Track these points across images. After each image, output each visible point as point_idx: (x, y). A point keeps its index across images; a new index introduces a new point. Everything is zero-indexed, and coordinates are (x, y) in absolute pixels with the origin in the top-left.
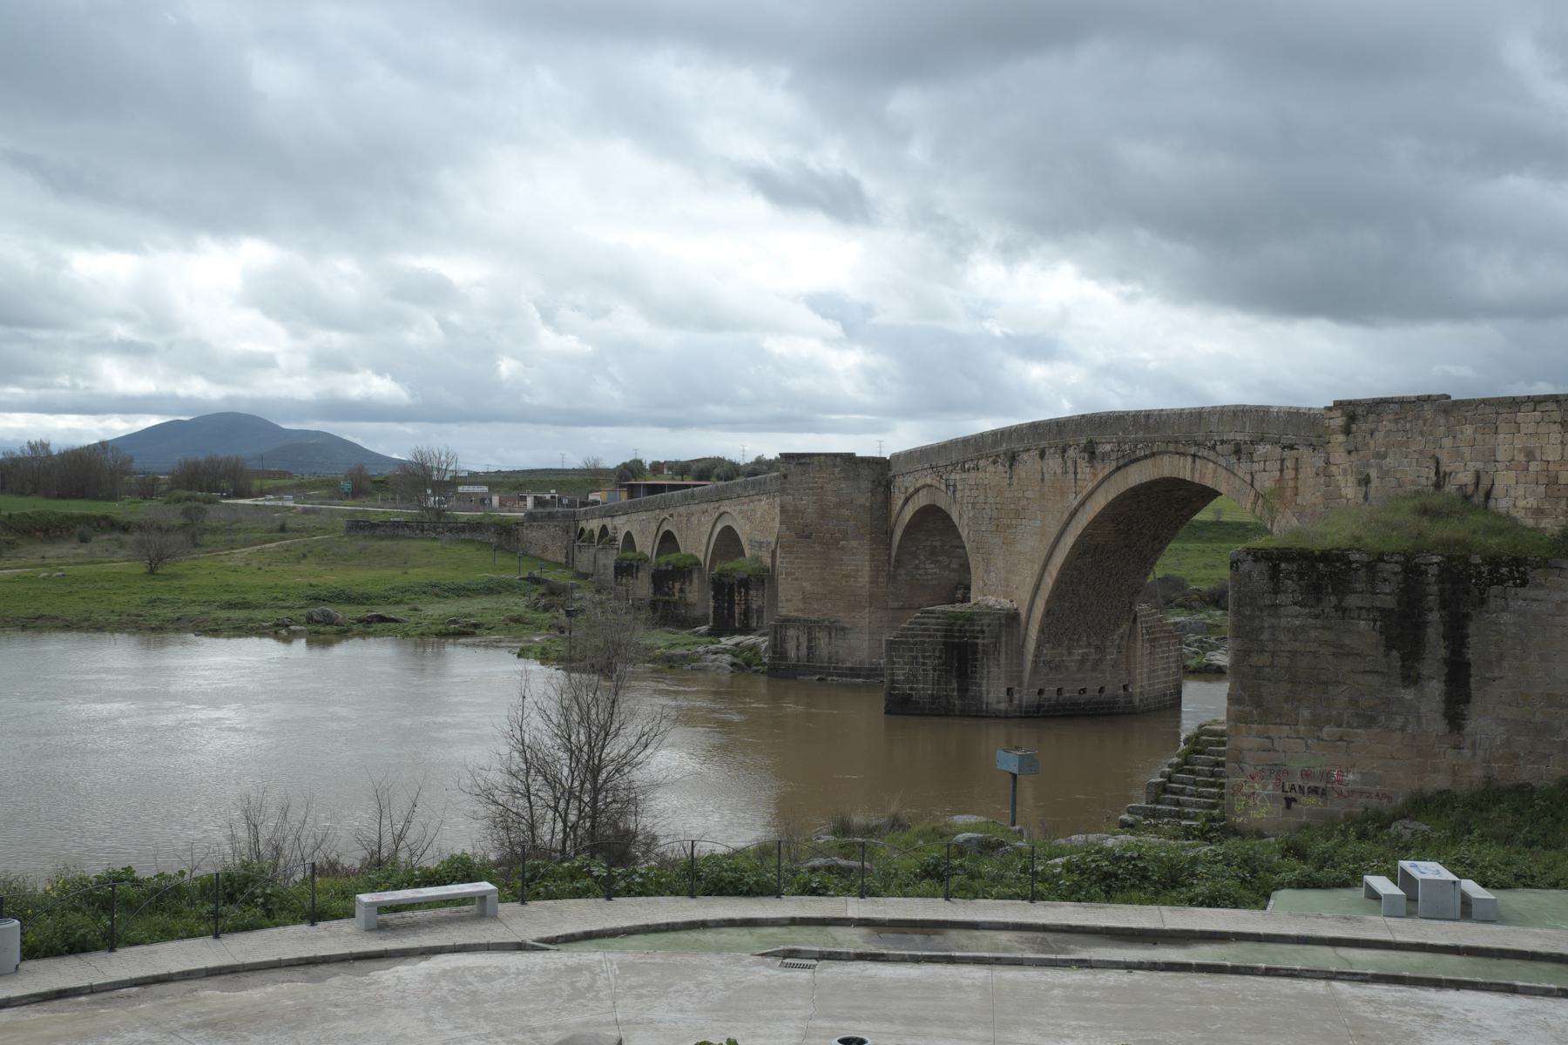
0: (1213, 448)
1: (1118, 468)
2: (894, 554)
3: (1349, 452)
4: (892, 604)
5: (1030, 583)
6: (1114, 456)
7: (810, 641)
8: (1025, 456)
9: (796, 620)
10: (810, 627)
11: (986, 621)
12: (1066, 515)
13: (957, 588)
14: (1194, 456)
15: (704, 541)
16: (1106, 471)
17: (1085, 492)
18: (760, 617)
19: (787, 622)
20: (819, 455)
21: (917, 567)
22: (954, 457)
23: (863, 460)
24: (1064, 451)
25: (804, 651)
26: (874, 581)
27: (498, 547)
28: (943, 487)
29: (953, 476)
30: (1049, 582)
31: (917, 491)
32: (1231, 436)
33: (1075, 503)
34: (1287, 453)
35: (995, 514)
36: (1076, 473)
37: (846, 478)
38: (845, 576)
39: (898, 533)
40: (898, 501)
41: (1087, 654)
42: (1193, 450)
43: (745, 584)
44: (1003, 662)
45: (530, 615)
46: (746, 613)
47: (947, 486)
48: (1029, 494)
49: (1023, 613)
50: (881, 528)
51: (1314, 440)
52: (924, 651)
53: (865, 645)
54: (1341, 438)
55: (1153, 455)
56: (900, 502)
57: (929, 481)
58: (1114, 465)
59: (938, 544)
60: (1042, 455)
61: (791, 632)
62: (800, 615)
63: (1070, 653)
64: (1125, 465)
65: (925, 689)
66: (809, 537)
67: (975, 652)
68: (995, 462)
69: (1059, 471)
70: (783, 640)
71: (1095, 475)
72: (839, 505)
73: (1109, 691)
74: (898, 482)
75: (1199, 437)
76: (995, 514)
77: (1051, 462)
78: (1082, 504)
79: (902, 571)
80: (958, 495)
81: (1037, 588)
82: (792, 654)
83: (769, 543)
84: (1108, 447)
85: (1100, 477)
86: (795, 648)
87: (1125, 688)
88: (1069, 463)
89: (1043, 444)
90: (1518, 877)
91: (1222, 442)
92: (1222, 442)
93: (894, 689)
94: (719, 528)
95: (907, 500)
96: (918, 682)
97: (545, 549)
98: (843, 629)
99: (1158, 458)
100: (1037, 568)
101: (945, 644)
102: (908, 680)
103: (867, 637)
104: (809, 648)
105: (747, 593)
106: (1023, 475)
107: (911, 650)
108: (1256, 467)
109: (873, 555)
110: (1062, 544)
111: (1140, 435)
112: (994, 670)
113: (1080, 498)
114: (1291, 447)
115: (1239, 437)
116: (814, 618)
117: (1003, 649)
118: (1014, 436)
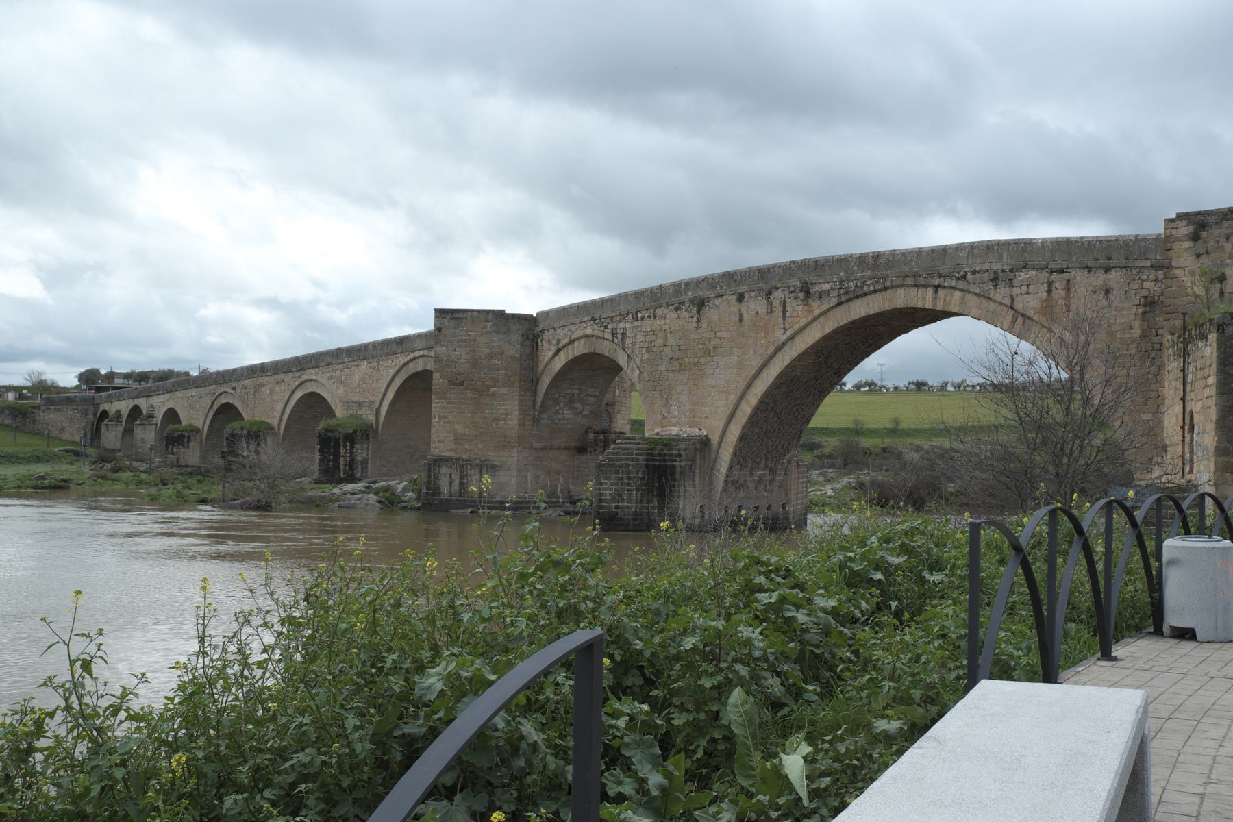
0: (964, 277)
1: (839, 304)
2: (539, 400)
3: (1198, 256)
4: (536, 445)
5: (723, 411)
6: (836, 293)
7: (462, 477)
8: (718, 302)
9: (449, 459)
10: (462, 465)
11: (683, 446)
12: (771, 349)
13: (587, 432)
14: (937, 287)
15: (279, 408)
16: (824, 308)
17: (796, 327)
18: (364, 468)
19: (440, 461)
20: (472, 311)
21: (557, 413)
22: (623, 309)
23: (514, 316)
24: (769, 293)
25: (456, 487)
26: (522, 424)
27: (17, 429)
28: (609, 336)
29: (621, 325)
30: (747, 409)
31: (572, 342)
32: (986, 266)
33: (784, 337)
34: (1055, 276)
35: (678, 354)
36: (784, 311)
37: (498, 332)
38: (495, 419)
39: (545, 381)
40: (547, 352)
41: (763, 475)
42: (937, 281)
43: (351, 438)
44: (697, 482)
45: (110, 474)
46: (351, 465)
47: (613, 335)
48: (723, 334)
49: (715, 440)
50: (529, 380)
51: (1090, 263)
52: (629, 472)
53: (514, 481)
54: (1187, 244)
55: (885, 289)
56: (551, 354)
57: (589, 331)
58: (835, 301)
59: (576, 392)
60: (741, 298)
61: (444, 470)
62: (453, 454)
63: (751, 474)
64: (848, 301)
65: (629, 507)
66: (462, 384)
67: (673, 474)
68: (677, 309)
69: (762, 311)
70: (437, 478)
71: (810, 312)
72: (490, 356)
73: (774, 509)
74: (548, 335)
75: (945, 270)
76: (678, 354)
77: (752, 305)
78: (792, 338)
79: (545, 416)
80: (627, 341)
81: (732, 416)
82: (445, 490)
83: (372, 402)
84: (827, 287)
85: (816, 312)
86: (447, 484)
87: (784, 508)
88: (776, 303)
89: (741, 289)
90: (928, 700)
91: (974, 272)
92: (974, 272)
93: (601, 507)
94: (298, 394)
95: (558, 351)
96: (623, 501)
97: (62, 430)
98: (494, 467)
99: (889, 292)
100: (733, 398)
101: (647, 466)
102: (614, 500)
103: (515, 474)
104: (462, 484)
105: (352, 447)
106: (715, 318)
107: (617, 472)
108: (1016, 291)
109: (521, 401)
110: (763, 375)
111: (869, 273)
112: (690, 489)
113: (789, 333)
114: (1061, 271)
115: (994, 267)
116: (465, 457)
117: (697, 471)
118: (703, 284)
